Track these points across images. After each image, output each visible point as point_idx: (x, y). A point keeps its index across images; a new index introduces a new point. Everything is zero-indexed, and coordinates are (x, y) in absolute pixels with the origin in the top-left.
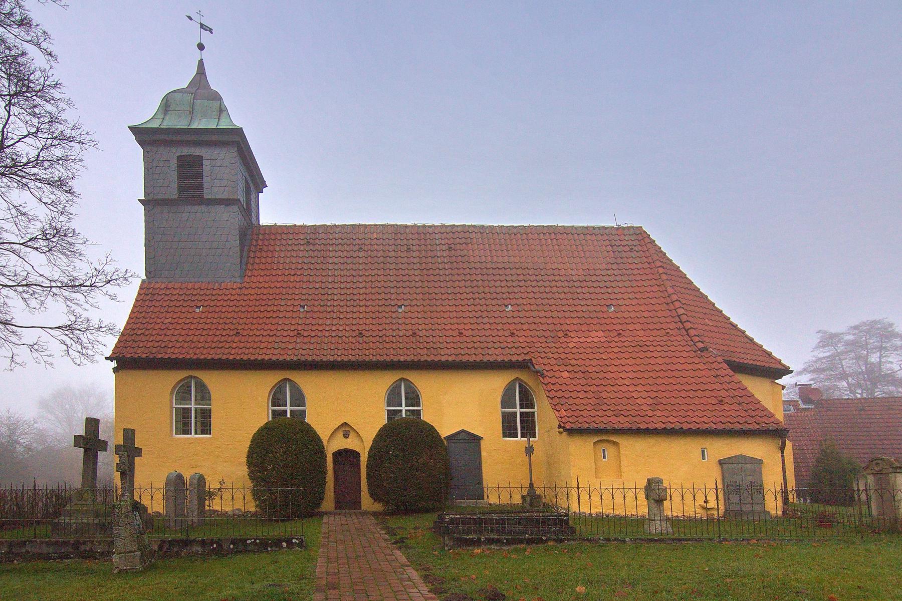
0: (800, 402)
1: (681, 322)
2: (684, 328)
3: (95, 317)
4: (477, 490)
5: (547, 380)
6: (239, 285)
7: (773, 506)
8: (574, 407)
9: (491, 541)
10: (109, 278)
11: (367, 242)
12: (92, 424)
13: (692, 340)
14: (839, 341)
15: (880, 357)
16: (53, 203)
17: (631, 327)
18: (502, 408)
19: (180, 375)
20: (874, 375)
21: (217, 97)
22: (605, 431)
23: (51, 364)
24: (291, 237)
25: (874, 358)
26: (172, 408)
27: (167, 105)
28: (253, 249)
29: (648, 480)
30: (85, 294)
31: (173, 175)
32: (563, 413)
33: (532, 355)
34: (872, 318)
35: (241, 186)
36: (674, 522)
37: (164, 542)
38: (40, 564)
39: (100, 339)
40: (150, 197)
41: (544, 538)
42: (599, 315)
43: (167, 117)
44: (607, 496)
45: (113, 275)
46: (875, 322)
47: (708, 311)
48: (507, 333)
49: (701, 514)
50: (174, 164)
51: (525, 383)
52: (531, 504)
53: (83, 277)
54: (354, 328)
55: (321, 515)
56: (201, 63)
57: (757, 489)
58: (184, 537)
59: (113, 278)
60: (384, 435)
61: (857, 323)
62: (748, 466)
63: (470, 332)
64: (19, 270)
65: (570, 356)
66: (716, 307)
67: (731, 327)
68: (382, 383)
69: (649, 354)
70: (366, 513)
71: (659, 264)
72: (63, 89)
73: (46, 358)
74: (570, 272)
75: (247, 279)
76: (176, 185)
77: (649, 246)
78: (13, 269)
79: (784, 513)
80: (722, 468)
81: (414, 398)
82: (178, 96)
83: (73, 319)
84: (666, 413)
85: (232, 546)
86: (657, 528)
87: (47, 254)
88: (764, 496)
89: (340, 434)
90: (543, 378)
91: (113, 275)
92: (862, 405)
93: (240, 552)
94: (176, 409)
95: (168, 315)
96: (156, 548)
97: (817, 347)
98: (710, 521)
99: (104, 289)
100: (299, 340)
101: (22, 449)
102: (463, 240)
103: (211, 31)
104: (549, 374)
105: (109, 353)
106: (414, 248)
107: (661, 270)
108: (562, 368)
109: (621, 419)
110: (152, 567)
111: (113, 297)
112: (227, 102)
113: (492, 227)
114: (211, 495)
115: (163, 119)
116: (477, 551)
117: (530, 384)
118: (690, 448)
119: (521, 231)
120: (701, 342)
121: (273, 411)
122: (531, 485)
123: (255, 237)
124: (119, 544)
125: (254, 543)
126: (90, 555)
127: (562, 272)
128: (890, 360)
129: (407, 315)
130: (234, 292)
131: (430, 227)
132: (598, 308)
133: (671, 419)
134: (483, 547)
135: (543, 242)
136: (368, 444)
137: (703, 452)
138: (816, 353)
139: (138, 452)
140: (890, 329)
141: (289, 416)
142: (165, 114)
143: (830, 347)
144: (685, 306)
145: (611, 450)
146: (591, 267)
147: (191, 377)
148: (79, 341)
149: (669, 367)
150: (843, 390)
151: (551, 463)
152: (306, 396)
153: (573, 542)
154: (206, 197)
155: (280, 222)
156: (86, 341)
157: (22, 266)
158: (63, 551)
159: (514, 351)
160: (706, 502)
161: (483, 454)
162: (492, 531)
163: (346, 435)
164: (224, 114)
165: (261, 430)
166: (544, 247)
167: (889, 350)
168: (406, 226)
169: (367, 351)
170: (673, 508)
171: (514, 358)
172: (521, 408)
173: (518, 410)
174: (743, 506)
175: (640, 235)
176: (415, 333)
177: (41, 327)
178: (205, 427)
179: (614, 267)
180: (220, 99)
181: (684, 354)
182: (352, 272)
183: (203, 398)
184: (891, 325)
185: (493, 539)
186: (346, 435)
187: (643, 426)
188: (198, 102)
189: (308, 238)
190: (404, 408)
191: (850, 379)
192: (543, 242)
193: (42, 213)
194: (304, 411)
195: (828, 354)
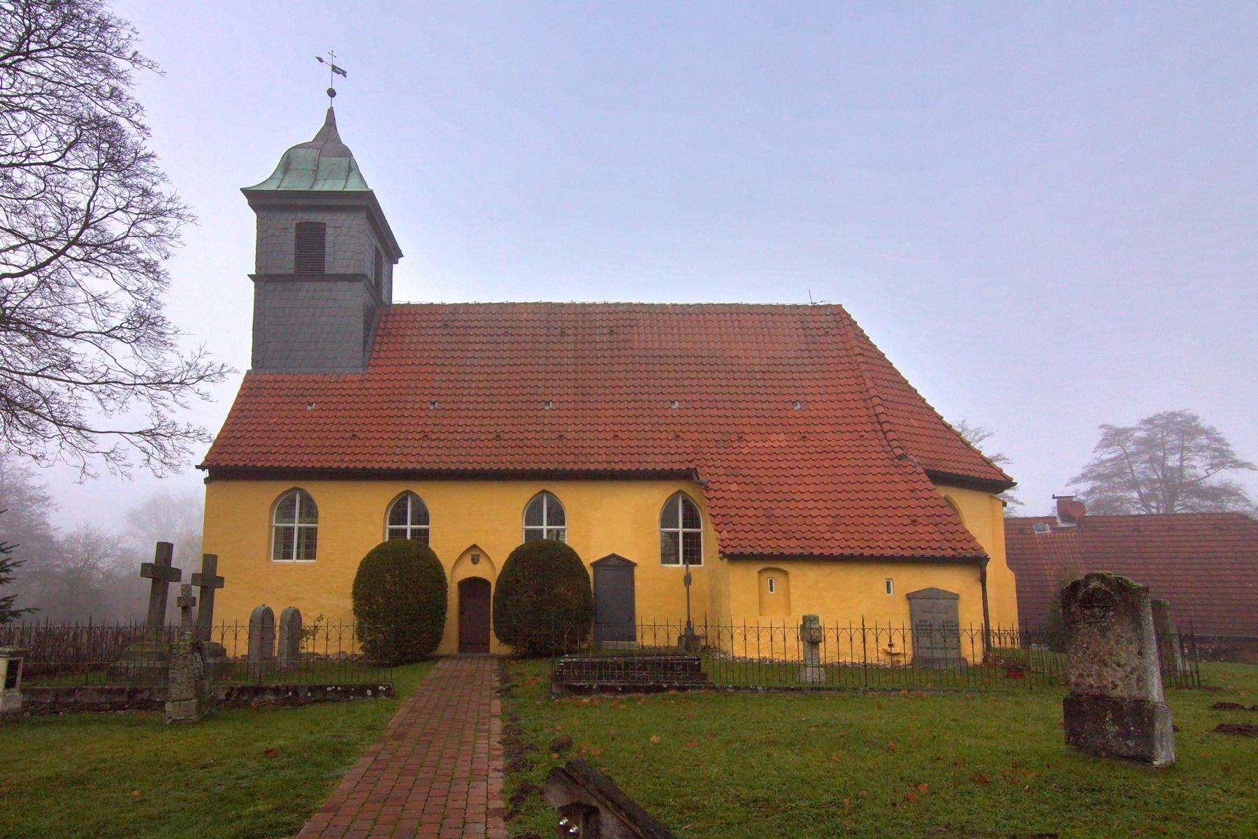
0: (1059, 520)
1: (879, 422)
2: (882, 430)
3: (182, 419)
4: (627, 625)
5: (711, 494)
6: (360, 377)
7: (972, 651)
8: (739, 528)
9: (603, 689)
10: (201, 373)
11: (514, 324)
12: (165, 549)
13: (889, 446)
14: (1128, 439)
15: (1182, 459)
16: (139, 291)
17: (818, 429)
18: (662, 527)
19: (280, 488)
20: (1174, 484)
21: (346, 153)
23: (129, 476)
24: (425, 318)
25: (1173, 461)
26: (271, 527)
27: (288, 163)
28: (380, 332)
29: (804, 618)
30: (174, 392)
31: (289, 244)
33: (698, 463)
34: (1169, 408)
35: (369, 256)
36: (829, 668)
37: (232, 689)
38: (87, 715)
39: (187, 446)
40: (262, 273)
41: (665, 686)
42: (783, 414)
43: (287, 177)
44: (765, 639)
45: (206, 370)
46: (1174, 415)
47: (916, 409)
48: (671, 436)
49: (885, 661)
50: (293, 231)
51: (689, 496)
52: (687, 647)
53: (173, 372)
54: (491, 429)
56: (331, 112)
57: (952, 630)
59: (207, 373)
60: (517, 558)
61: (1151, 416)
62: (942, 601)
63: (627, 435)
64: (97, 364)
65: (742, 465)
66: (926, 404)
67: (945, 429)
68: (517, 498)
69: (835, 463)
70: (494, 656)
71: (857, 351)
72: (157, 162)
73: (124, 469)
74: (752, 361)
75: (371, 370)
76: (292, 258)
77: (848, 328)
78: (89, 365)
79: (985, 660)
80: (911, 605)
81: (557, 516)
82: (302, 152)
83: (157, 422)
84: (848, 536)
85: (309, 694)
86: (809, 675)
87: (133, 344)
88: (958, 638)
89: (468, 559)
90: (707, 490)
91: (206, 370)
92: (1168, 523)
93: (319, 701)
94: (276, 528)
95: (275, 414)
96: (222, 696)
97: (1100, 446)
98: (895, 669)
99: (196, 387)
100: (425, 444)
101: (101, 576)
102: (628, 322)
103: (344, 74)
104: (715, 487)
105: (200, 461)
106: (570, 332)
107: (860, 359)
108: (730, 479)
109: (793, 543)
111: (205, 397)
112: (357, 157)
113: (663, 306)
115: (282, 180)
116: (586, 700)
117: (696, 500)
118: (874, 578)
119: (697, 311)
120: (901, 448)
124: (175, 690)
125: (335, 691)
126: (146, 705)
127: (742, 361)
128: (1194, 463)
129: (554, 414)
130: (353, 386)
131: (590, 305)
133: (852, 543)
134: (595, 696)
135: (723, 323)
136: (499, 570)
137: (888, 584)
138: (1098, 454)
139: (220, 582)
140: (1193, 424)
141: (409, 537)
143: (1116, 447)
144: (885, 404)
145: (779, 580)
146: (778, 354)
148: (162, 448)
149: (858, 478)
150: (1133, 503)
151: (715, 596)
152: (430, 512)
153: (697, 691)
154: (327, 271)
155: (414, 301)
156: (171, 448)
157: (102, 360)
158: (116, 700)
159: (677, 458)
160: (891, 645)
161: (637, 584)
162: (619, 677)
163: (475, 561)
164: (353, 173)
166: (724, 330)
167: (1191, 452)
168: (562, 305)
169: (504, 458)
170: (829, 652)
171: (676, 467)
172: (684, 527)
173: (681, 530)
174: (934, 651)
175: (838, 316)
176: (561, 436)
177: (120, 433)
178: (309, 550)
179: (805, 354)
180: (350, 155)
181: (878, 463)
182: (494, 361)
184: (1194, 418)
185: (607, 687)
186: (475, 561)
187: (816, 552)
188: (323, 159)
189: (446, 319)
190: (545, 527)
191: (1143, 490)
192: (723, 323)
193: (126, 302)
194: (427, 531)
195: (1113, 455)
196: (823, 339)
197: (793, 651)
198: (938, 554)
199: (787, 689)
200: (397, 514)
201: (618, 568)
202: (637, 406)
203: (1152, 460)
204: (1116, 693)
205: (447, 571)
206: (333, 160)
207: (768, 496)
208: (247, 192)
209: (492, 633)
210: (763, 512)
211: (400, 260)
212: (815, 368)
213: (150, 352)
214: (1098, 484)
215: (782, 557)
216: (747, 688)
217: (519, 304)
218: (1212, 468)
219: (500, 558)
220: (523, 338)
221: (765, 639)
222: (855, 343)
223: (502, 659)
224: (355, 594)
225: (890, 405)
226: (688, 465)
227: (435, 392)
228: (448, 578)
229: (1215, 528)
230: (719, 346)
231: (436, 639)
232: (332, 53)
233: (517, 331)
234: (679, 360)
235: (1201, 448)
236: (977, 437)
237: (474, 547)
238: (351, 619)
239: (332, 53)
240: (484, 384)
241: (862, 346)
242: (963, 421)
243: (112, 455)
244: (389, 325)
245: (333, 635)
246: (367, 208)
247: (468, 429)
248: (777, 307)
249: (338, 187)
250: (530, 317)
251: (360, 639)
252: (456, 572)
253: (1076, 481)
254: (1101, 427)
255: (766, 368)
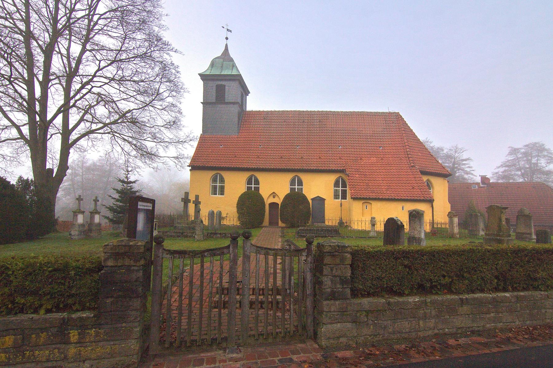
0: (481, 184)
4: (322, 219)
14: (518, 152)
19: (214, 172)
20: (535, 170)
21: (232, 60)
22: (366, 199)
25: (534, 161)
27: (213, 64)
32: (353, 191)
34: (534, 141)
35: (240, 95)
42: (376, 151)
44: (363, 224)
46: (536, 143)
50: (215, 88)
55: (262, 227)
56: (227, 45)
58: (215, 232)
60: (287, 197)
61: (527, 144)
65: (361, 168)
67: (430, 156)
68: (287, 178)
71: (403, 129)
75: (240, 134)
81: (300, 183)
86: (372, 234)
89: (272, 196)
94: (212, 185)
100: (258, 160)
107: (403, 132)
110: (204, 240)
113: (338, 112)
114: (223, 218)
121: (247, 187)
122: (341, 218)
123: (244, 116)
124: (197, 232)
127: (363, 132)
132: (375, 148)
137: (403, 207)
138: (507, 158)
140: (543, 147)
142: (212, 68)
145: (369, 206)
147: (218, 173)
148: (180, 162)
151: (350, 210)
154: (226, 101)
162: (315, 233)
163: (274, 197)
165: (242, 195)
168: (304, 111)
175: (397, 117)
176: (302, 157)
178: (222, 193)
179: (385, 130)
180: (233, 61)
183: (222, 181)
184: (543, 145)
186: (274, 197)
190: (296, 187)
195: (513, 158)
196: (392, 125)
197: (368, 227)
198: (418, 198)
199: (361, 238)
200: (249, 182)
201: (320, 201)
202: (327, 147)
203: (527, 160)
204: (416, 236)
205: (265, 201)
206: (227, 63)
207: (368, 179)
208: (200, 75)
209: (279, 219)
210: (366, 184)
211: (249, 94)
212: (388, 135)
213: (174, 132)
214: (507, 168)
215: (370, 199)
216: (350, 237)
217: (289, 111)
218: (548, 164)
219: (282, 195)
220: (290, 123)
221: (363, 224)
222: (402, 126)
223: (282, 228)
224: (237, 207)
225: (411, 148)
226: (343, 168)
227: (261, 142)
228: (266, 202)
229: (533, 188)
230: (356, 127)
231: (262, 221)
232: (227, 25)
233: (288, 121)
234: (342, 132)
235: (544, 156)
236: (461, 151)
237: (274, 193)
238: (236, 215)
239: (227, 25)
240: (277, 139)
241: (404, 127)
242: (457, 145)
243: (165, 163)
244: (246, 118)
245: (232, 219)
246: (238, 80)
247: (272, 155)
248: (377, 113)
249: (229, 73)
250: (293, 115)
251: (239, 220)
252: (268, 201)
253: (499, 167)
254: (509, 147)
255: (371, 135)
